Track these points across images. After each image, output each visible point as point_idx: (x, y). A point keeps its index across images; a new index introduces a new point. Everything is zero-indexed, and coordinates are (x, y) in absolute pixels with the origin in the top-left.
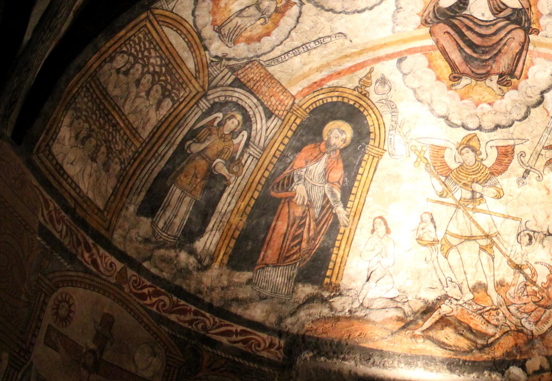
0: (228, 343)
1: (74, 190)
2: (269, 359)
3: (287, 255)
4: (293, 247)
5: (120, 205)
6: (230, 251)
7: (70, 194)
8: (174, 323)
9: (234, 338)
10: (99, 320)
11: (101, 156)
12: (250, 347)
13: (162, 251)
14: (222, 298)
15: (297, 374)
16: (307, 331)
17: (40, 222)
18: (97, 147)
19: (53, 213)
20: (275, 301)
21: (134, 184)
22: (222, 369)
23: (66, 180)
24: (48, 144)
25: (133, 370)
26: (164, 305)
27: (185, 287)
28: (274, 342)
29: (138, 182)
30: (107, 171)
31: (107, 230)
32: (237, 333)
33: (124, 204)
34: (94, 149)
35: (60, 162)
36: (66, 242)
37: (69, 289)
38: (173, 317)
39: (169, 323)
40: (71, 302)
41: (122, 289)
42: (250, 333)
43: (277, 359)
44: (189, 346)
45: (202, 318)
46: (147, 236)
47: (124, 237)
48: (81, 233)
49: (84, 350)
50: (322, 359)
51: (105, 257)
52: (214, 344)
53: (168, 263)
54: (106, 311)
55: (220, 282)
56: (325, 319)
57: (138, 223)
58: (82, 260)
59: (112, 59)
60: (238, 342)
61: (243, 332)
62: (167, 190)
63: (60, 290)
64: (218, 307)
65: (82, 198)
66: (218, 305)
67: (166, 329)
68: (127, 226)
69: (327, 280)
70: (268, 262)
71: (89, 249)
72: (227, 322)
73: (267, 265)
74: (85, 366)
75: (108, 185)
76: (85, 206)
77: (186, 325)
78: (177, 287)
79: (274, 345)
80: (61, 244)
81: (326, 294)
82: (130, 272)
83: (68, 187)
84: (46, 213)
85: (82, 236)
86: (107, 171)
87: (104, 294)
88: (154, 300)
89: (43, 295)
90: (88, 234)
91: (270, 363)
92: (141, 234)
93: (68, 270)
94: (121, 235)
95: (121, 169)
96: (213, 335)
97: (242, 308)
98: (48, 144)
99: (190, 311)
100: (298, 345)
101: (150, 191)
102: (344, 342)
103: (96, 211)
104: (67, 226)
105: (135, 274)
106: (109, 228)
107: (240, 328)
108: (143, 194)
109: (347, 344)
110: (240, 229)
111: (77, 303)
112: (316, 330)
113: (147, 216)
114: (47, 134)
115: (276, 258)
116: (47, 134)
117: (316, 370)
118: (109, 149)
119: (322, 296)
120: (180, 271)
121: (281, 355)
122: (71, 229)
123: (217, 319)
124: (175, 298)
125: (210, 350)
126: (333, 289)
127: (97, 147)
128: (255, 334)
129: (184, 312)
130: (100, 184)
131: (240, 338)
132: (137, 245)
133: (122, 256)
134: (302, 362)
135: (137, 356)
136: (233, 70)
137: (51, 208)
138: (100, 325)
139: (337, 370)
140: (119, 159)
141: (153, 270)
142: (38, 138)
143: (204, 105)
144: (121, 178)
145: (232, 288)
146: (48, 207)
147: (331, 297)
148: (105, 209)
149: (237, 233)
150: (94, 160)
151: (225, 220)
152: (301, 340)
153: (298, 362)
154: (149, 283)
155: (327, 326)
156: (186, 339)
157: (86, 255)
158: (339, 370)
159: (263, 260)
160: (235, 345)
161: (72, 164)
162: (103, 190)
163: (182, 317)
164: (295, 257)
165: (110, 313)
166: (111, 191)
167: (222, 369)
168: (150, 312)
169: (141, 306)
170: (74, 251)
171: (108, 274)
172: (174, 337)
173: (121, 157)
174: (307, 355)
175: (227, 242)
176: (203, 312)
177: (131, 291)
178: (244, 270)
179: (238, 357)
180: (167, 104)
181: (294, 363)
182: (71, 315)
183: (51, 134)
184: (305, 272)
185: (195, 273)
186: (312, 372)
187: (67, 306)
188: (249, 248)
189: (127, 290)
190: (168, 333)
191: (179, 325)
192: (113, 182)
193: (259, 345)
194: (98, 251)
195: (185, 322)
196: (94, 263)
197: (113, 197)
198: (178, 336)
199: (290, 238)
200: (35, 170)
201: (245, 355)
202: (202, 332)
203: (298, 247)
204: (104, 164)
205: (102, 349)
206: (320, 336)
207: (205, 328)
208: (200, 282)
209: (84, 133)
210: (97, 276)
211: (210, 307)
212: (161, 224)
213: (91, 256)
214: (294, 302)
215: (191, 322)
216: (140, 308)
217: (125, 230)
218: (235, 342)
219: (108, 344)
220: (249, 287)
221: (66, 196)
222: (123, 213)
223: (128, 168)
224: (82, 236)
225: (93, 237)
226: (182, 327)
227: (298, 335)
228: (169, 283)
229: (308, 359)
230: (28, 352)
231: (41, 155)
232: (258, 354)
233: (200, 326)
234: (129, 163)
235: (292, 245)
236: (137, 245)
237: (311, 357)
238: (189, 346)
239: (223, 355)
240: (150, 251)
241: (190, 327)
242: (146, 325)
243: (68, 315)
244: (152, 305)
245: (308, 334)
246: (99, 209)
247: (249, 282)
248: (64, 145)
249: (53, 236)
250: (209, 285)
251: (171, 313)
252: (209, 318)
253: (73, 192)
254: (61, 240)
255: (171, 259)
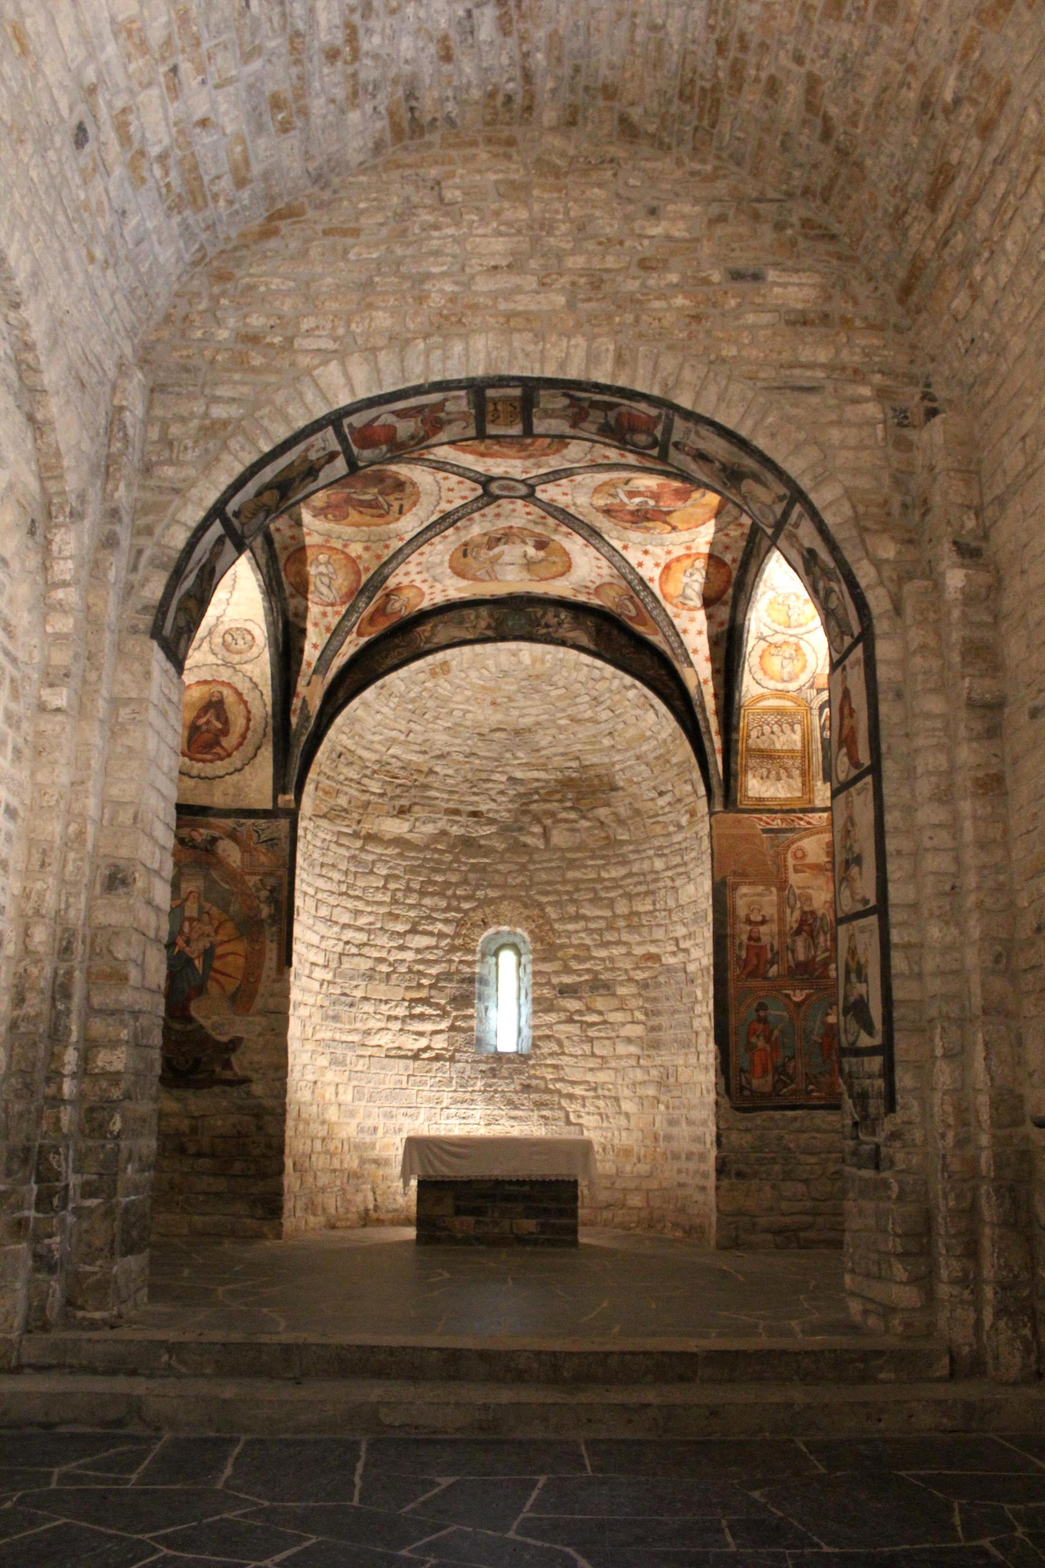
18: (778, 773)
37: (799, 844)
48: (792, 816)
59: (749, 736)
71: (801, 819)
75: (797, 782)
118: (786, 769)
127: (778, 773)
136: (811, 687)
143: (816, 712)
180: (797, 727)
192: (799, 780)
196: (809, 823)
209: (765, 774)
230: (786, 881)
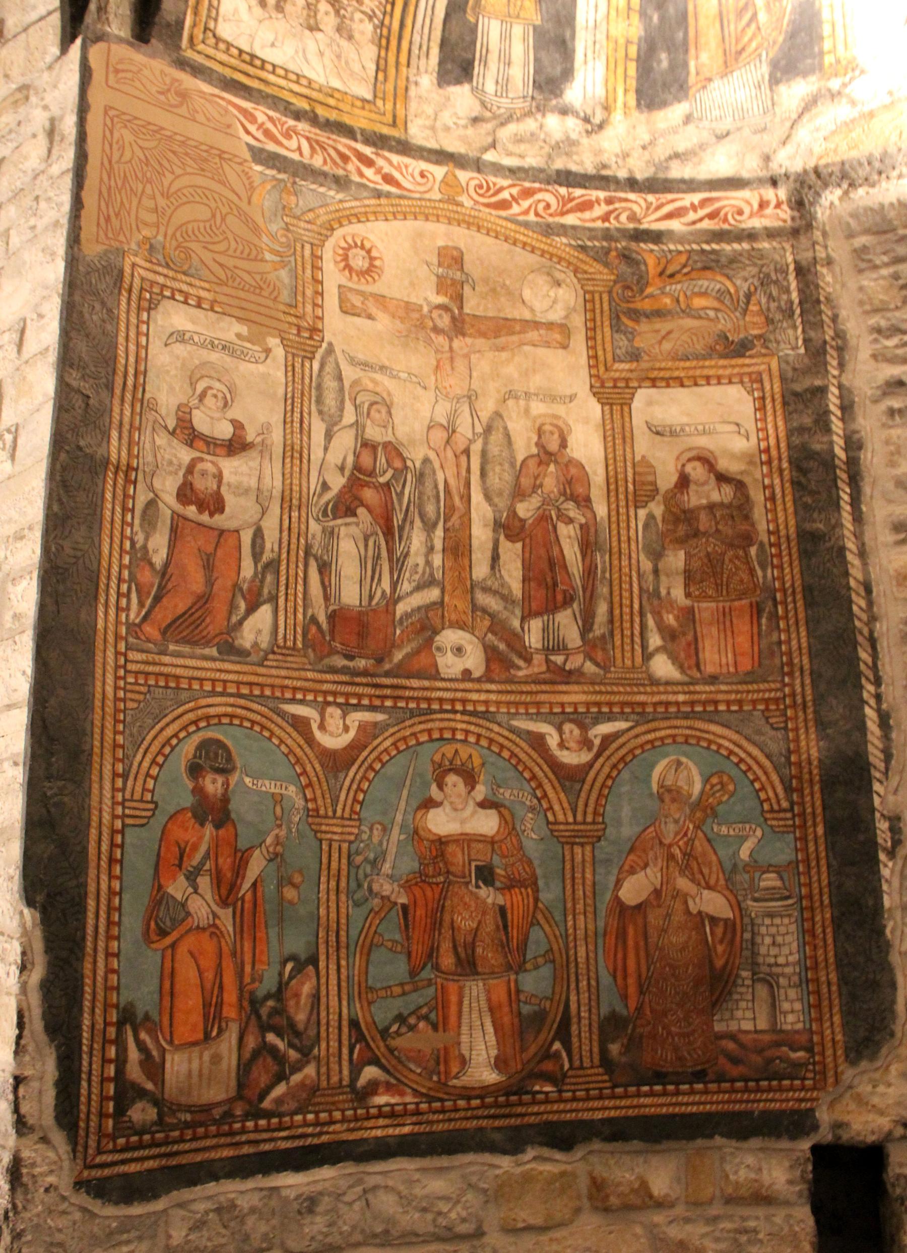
0: (684, 229)
1: (297, 82)
2: (766, 228)
3: (740, 47)
4: (743, 30)
5: (402, 84)
6: (633, 84)
7: (292, 91)
8: (574, 228)
9: (692, 216)
10: (435, 260)
11: (326, 19)
12: (725, 220)
13: (512, 128)
14: (648, 162)
15: (825, 234)
16: (821, 158)
17: (247, 144)
19: (269, 125)
20: (746, 132)
21: (411, 43)
22: (685, 270)
23: (273, 72)
24: (206, 29)
25: (527, 315)
26: (548, 206)
27: (574, 168)
28: (765, 198)
29: (417, 38)
30: (350, 38)
31: (394, 124)
32: (694, 208)
33: (407, 79)
34: (305, 12)
35: (246, 48)
36: (318, 162)
37: (357, 229)
38: (571, 220)
39: (564, 230)
40: (367, 245)
41: (460, 205)
42: (718, 199)
43: (781, 224)
44: (614, 253)
45: (623, 205)
46: (474, 115)
47: (433, 128)
48: (343, 143)
49: (426, 309)
50: (861, 191)
51: (406, 167)
52: (656, 237)
53: (529, 142)
54: (441, 243)
55: (635, 139)
56: (849, 125)
57: (448, 99)
58: (364, 181)
60: (701, 220)
61: (704, 203)
62: (474, 30)
63: (339, 233)
64: (647, 180)
65: (320, 91)
66: (647, 175)
67: (564, 240)
68: (430, 111)
69: (828, 59)
70: (708, 75)
71: (370, 163)
72: (670, 196)
73: (710, 80)
74: (436, 330)
76: (332, 102)
77: (599, 224)
78: (558, 172)
79: (768, 203)
80: (305, 167)
81: (834, 84)
82: (463, 176)
83: (283, 82)
84: (252, 128)
85: (346, 146)
86: (350, 38)
87: (427, 219)
88: (525, 204)
89: (308, 247)
90: (356, 140)
91: (771, 234)
92: (461, 114)
93: (341, 201)
94: (425, 127)
95: (375, 27)
96: (650, 223)
97: (690, 164)
98: (206, 29)
99: (598, 201)
100: (810, 187)
101: (443, 44)
102: (892, 150)
103: (359, 104)
104: (308, 139)
105: (475, 175)
106: (394, 122)
107: (696, 198)
108: (435, 51)
109: (900, 150)
110: (636, 40)
111: (379, 245)
112: (835, 151)
113: (458, 82)
114: (196, 13)
115: (721, 61)
116: (196, 13)
117: (854, 215)
119: (829, 90)
120: (557, 146)
121: (786, 213)
122: (317, 142)
123: (651, 198)
124: (563, 191)
125: (655, 248)
126: (846, 69)
128: (727, 198)
129: (586, 206)
130: (347, 63)
131: (701, 213)
132: (461, 132)
133: (441, 156)
134: (828, 212)
135: (527, 294)
137: (261, 118)
138: (440, 265)
139: (895, 201)
140: (363, 12)
141: (508, 162)
142: (180, 24)
144: (383, 41)
145: (662, 140)
146: (253, 119)
147: (845, 85)
148: (375, 96)
149: (633, 51)
150: (314, 28)
151: (601, 37)
152: (813, 176)
153: (819, 215)
154: (505, 183)
155: (853, 135)
156: (605, 244)
157: (369, 172)
158: (899, 201)
159: (697, 74)
160: (699, 226)
161: (273, 45)
162: (357, 67)
163: (587, 215)
164: (754, 45)
165: (450, 244)
166: (373, 67)
167: (685, 270)
168: (526, 225)
169: (506, 219)
170: (341, 172)
171: (422, 189)
172: (583, 248)
173: (364, 8)
174: (832, 196)
175: (620, 71)
176: (622, 195)
177: (476, 202)
178: (671, 104)
179: (708, 243)
181: (813, 217)
182: (377, 263)
183: (204, 12)
184: (783, 63)
185: (585, 141)
186: (851, 221)
187: (359, 251)
188: (665, 64)
189: (468, 203)
190: (570, 245)
191: (585, 228)
192: (370, 53)
193: (740, 212)
194: (390, 163)
195: (593, 220)
196: (388, 179)
197: (381, 76)
198: (589, 244)
199: (732, 17)
200: (197, 71)
201: (719, 236)
202: (631, 226)
203: (753, 26)
204: (339, 30)
205: (459, 299)
206: (845, 157)
207: (633, 218)
208: (598, 152)
210: (400, 197)
211: (632, 184)
212: (490, 87)
213: (379, 171)
214: (782, 121)
215: (605, 218)
216: (504, 223)
217: (428, 117)
218: (694, 223)
219: (467, 289)
220: (691, 127)
221: (286, 95)
222: (413, 92)
223: (387, 22)
224: (346, 146)
225: (367, 141)
226: (590, 230)
227: (805, 171)
228: (542, 171)
229: (837, 202)
231: (201, 47)
232: (743, 226)
233: (623, 218)
234: (385, 14)
235: (740, 27)
236: (461, 132)
237: (841, 199)
238: (614, 253)
239: (680, 248)
240: (488, 134)
241: (607, 225)
242: (525, 245)
243: (372, 265)
244: (526, 212)
245: (822, 162)
246: (364, 100)
247: (688, 119)
248: (241, 21)
249: (292, 162)
250: (618, 150)
251: (563, 214)
252: (637, 201)
253: (296, 88)
254: (306, 161)
255: (532, 134)
